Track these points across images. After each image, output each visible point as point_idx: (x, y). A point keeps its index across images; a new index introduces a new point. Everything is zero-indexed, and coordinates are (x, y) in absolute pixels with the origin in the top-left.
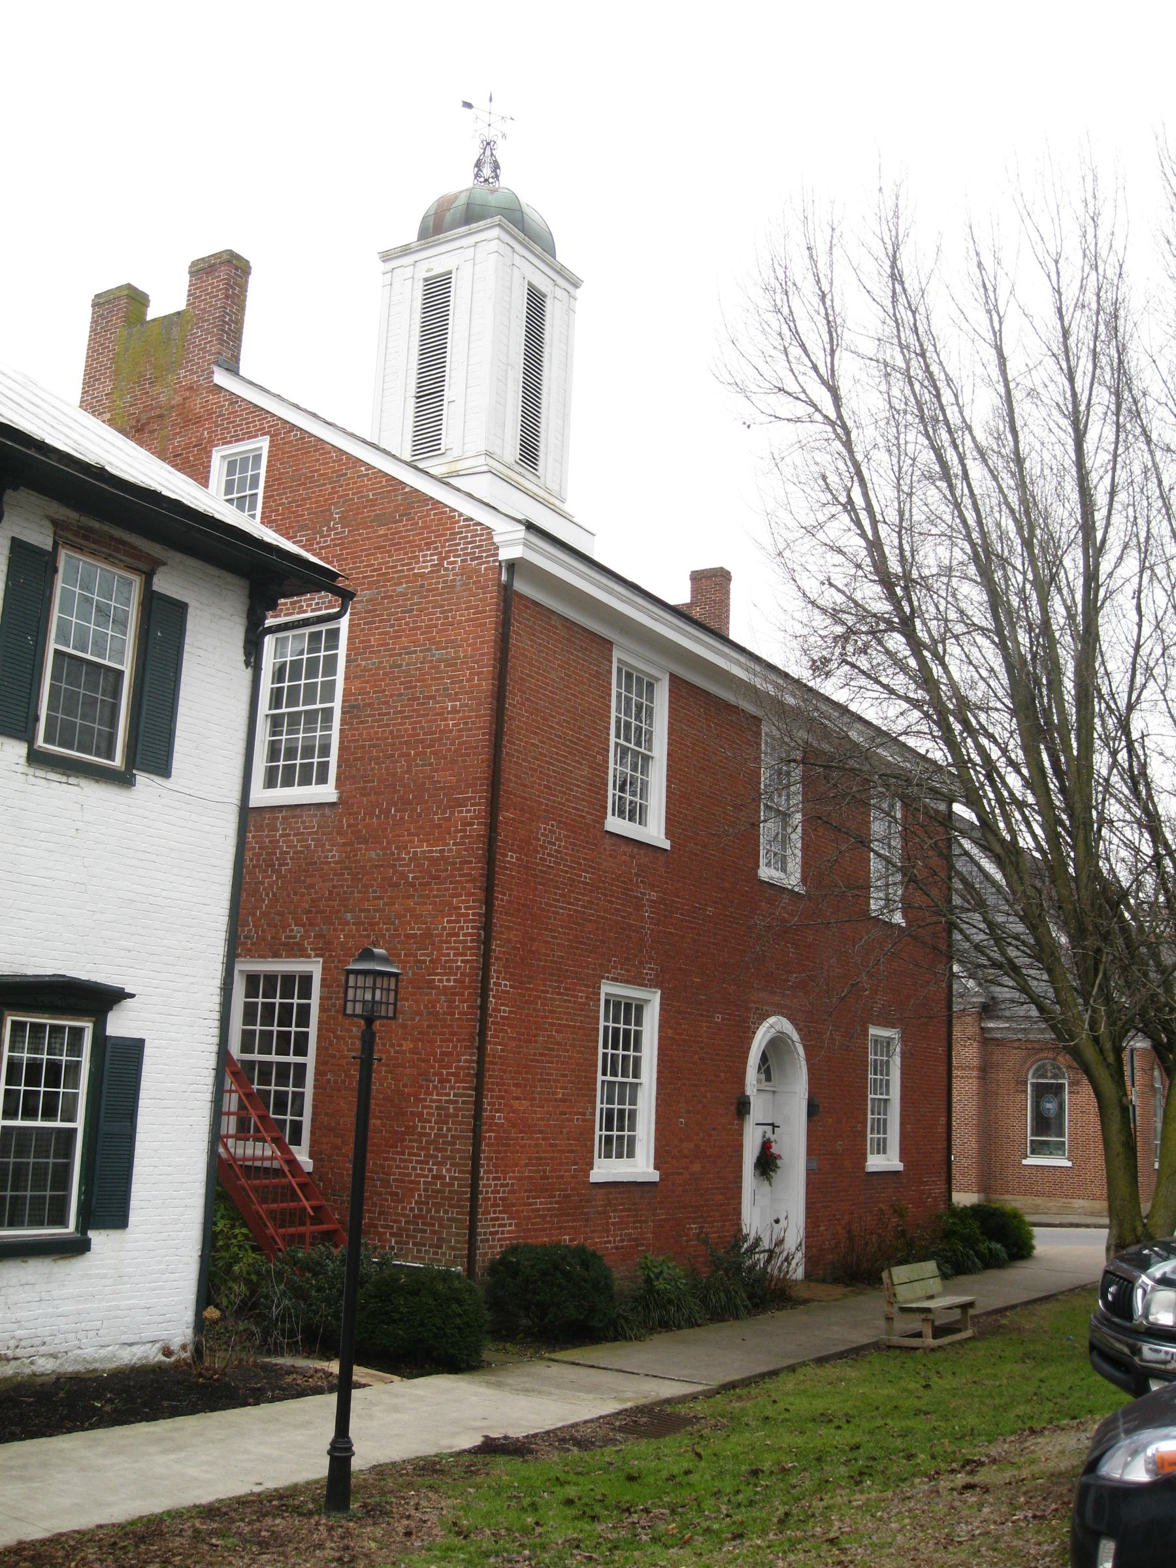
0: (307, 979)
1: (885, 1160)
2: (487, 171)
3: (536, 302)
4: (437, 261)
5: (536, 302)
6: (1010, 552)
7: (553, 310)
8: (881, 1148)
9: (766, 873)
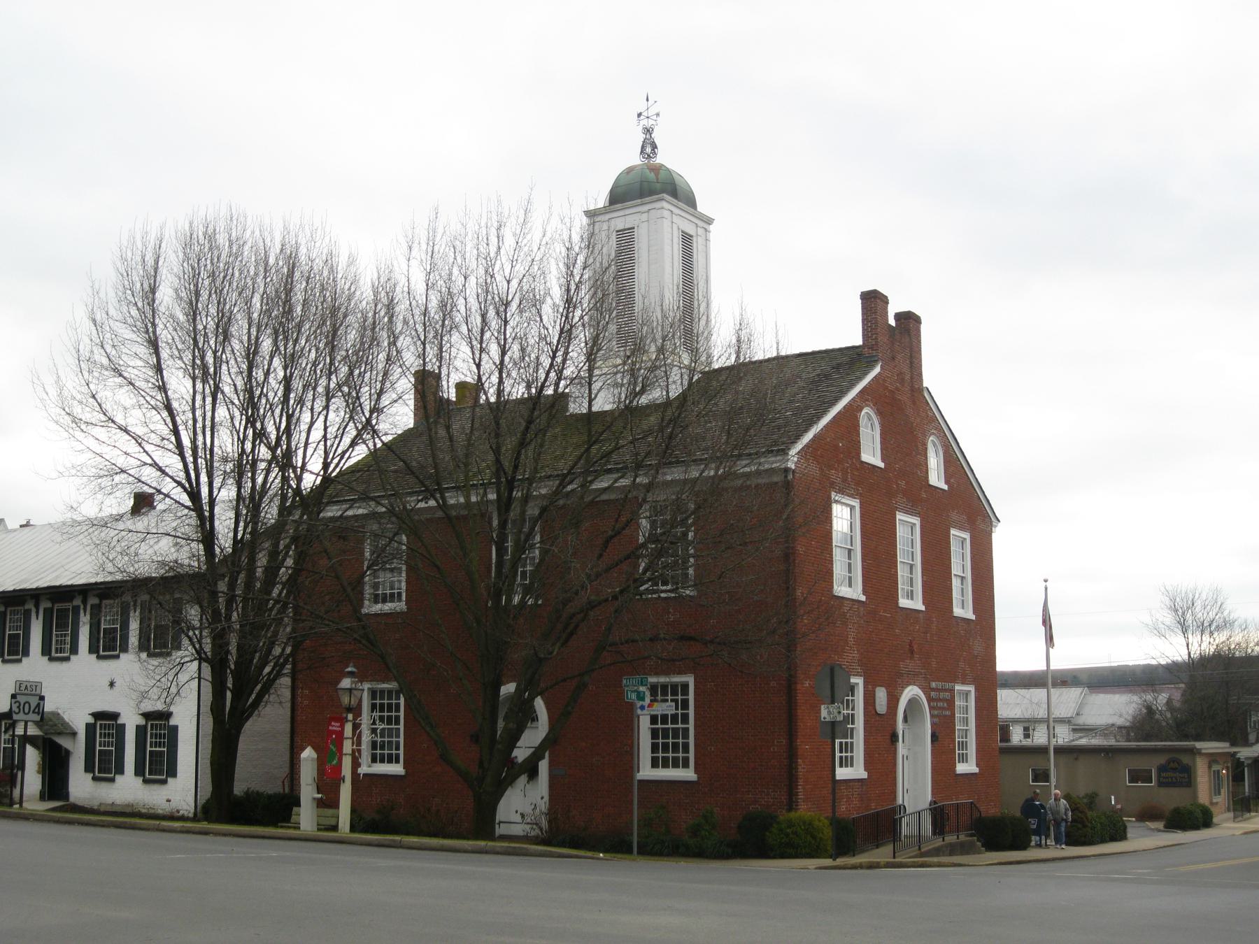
0: (685, 687)
1: (968, 766)
2: (648, 150)
3: (687, 239)
4: (622, 220)
5: (687, 239)
6: (440, 358)
7: (698, 244)
8: (964, 759)
9: (904, 602)
